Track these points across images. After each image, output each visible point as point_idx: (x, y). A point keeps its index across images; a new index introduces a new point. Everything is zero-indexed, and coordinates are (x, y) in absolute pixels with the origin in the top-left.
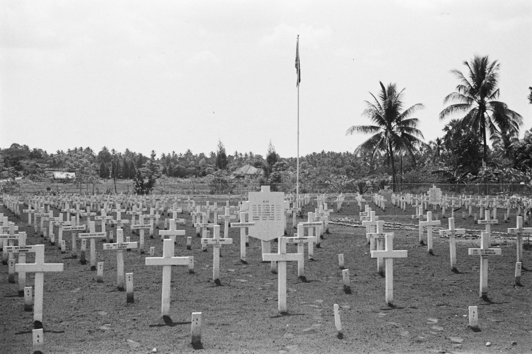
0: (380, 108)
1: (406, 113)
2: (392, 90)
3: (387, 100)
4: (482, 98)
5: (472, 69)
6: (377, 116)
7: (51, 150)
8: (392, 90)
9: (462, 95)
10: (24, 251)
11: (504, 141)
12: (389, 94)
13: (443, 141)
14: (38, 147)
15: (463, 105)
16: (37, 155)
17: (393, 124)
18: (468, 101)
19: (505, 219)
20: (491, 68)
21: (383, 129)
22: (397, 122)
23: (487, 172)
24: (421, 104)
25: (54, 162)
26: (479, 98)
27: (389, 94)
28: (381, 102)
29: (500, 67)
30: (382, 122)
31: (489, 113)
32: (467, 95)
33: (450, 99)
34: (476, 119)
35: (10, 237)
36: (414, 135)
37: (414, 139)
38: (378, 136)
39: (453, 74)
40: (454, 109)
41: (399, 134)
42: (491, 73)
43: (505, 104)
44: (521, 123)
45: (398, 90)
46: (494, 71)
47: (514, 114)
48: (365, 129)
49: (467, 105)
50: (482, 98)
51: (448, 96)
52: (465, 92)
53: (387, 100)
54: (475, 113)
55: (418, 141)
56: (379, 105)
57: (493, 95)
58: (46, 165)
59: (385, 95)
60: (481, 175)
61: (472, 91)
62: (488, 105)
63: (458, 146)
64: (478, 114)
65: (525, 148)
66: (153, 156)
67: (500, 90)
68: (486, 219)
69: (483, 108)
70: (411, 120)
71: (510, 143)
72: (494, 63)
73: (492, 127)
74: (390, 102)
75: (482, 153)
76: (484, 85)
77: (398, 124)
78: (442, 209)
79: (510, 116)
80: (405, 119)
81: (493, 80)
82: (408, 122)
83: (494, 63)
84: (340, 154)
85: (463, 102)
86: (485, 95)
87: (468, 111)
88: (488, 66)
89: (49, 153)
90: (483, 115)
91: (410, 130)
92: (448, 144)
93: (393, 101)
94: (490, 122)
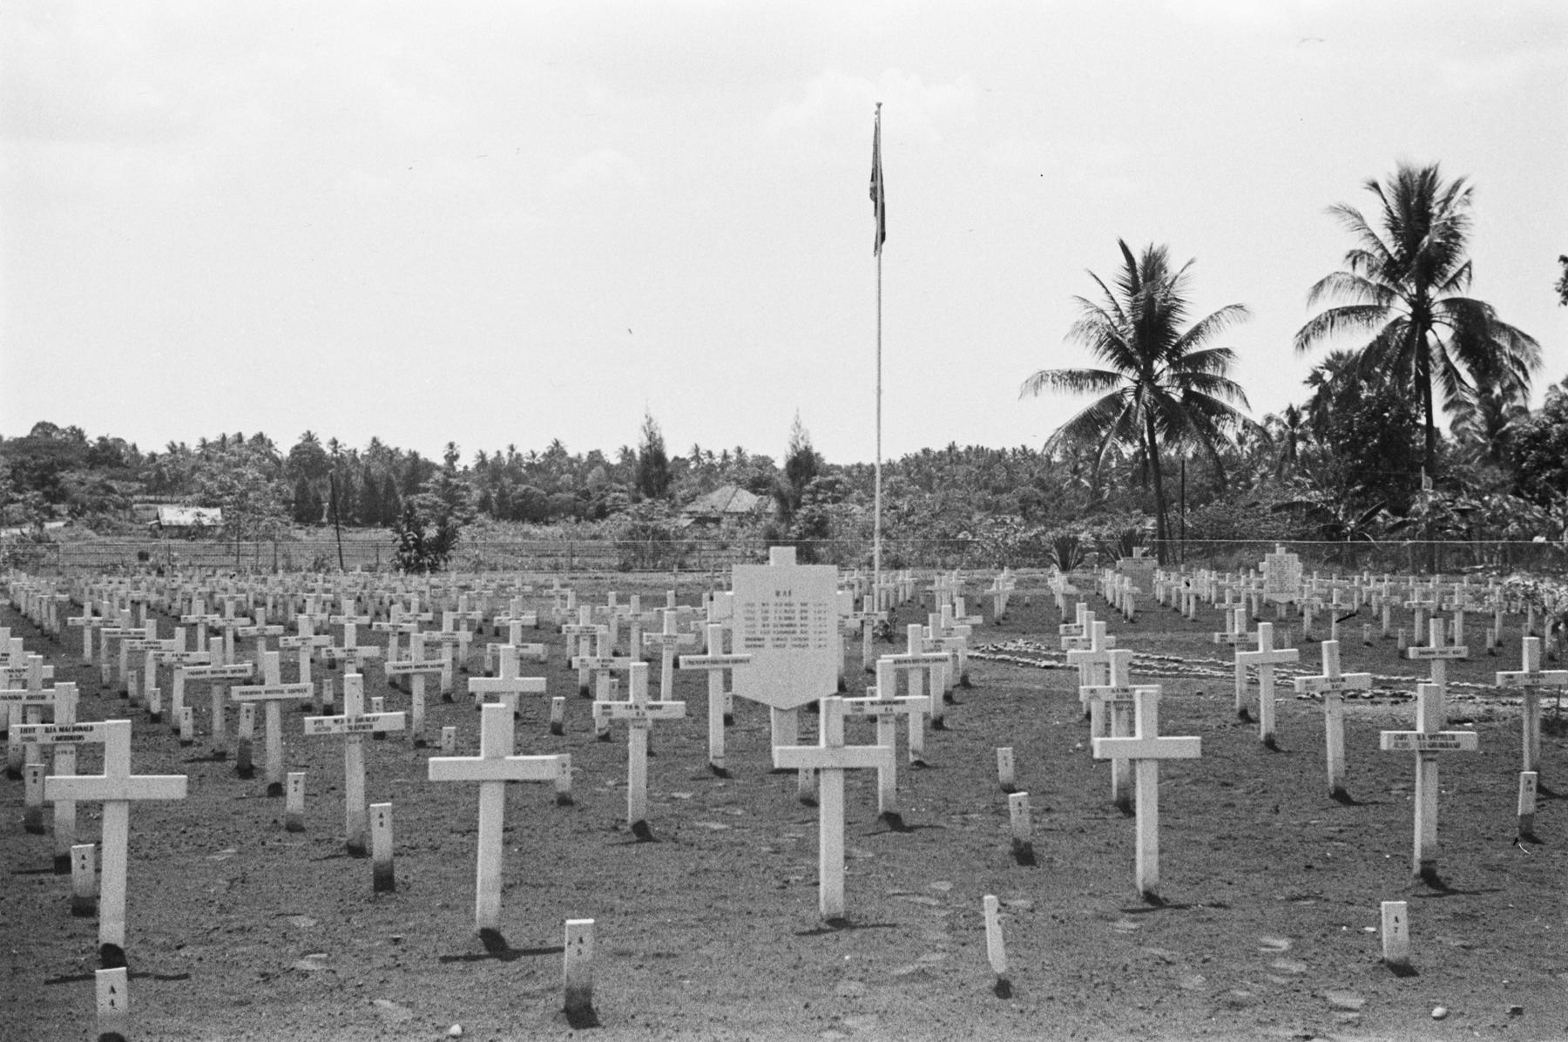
0: (1121, 317)
1: (1196, 332)
2: (1154, 264)
3: (1142, 295)
4: (1422, 288)
5: (1393, 203)
6: (1112, 343)
7: (150, 442)
8: (1154, 264)
9: (1361, 280)
10: (71, 738)
11: (1486, 414)
12: (1147, 276)
13: (1305, 416)
14: (112, 434)
15: (1363, 308)
16: (109, 455)
17: (1159, 366)
18: (1379, 296)
19: (1490, 643)
20: (1447, 200)
21: (1128, 380)
22: (1169, 359)
23: (1435, 507)
24: (1239, 307)
25: (160, 477)
26: (1412, 289)
27: (1147, 276)
28: (1124, 302)
29: (1474, 197)
30: (1125, 360)
31: (1441, 333)
32: (1376, 280)
33: (1327, 290)
34: (1404, 352)
35: (29, 698)
36: (1220, 396)
37: (1222, 410)
38: (1114, 401)
39: (1334, 218)
40: (1339, 320)
41: (1177, 395)
42: (1446, 215)
43: (1490, 308)
44: (1536, 363)
45: (1173, 265)
46: (1457, 209)
47: (1516, 336)
48: (1076, 379)
49: (1377, 310)
50: (1422, 288)
51: (1321, 283)
52: (1371, 271)
53: (1142, 295)
54: (1401, 332)
55: (1233, 414)
56: (1117, 309)
57: (1454, 281)
58: (136, 486)
59: (1135, 278)
60: (1417, 514)
61: (1392, 269)
62: (1437, 309)
63: (1350, 430)
64: (1410, 337)
65: (1548, 436)
66: (452, 458)
67: (1474, 266)
68: (1433, 645)
69: (1422, 317)
70: (1211, 352)
71: (1502, 421)
72: (1456, 187)
73: (1450, 374)
74: (1150, 300)
75: (1421, 451)
76: (1427, 250)
77: (1172, 365)
78: (1302, 614)
79: (1503, 341)
80: (1194, 349)
81: (1452, 234)
82: (1201, 358)
83: (1456, 187)
84: (1001, 454)
85: (1366, 300)
86: (1430, 281)
87: (1379, 327)
88: (1439, 195)
89: (144, 450)
90: (1424, 339)
91: (1208, 382)
92: (1320, 424)
93: (1159, 297)
94: (1445, 358)
